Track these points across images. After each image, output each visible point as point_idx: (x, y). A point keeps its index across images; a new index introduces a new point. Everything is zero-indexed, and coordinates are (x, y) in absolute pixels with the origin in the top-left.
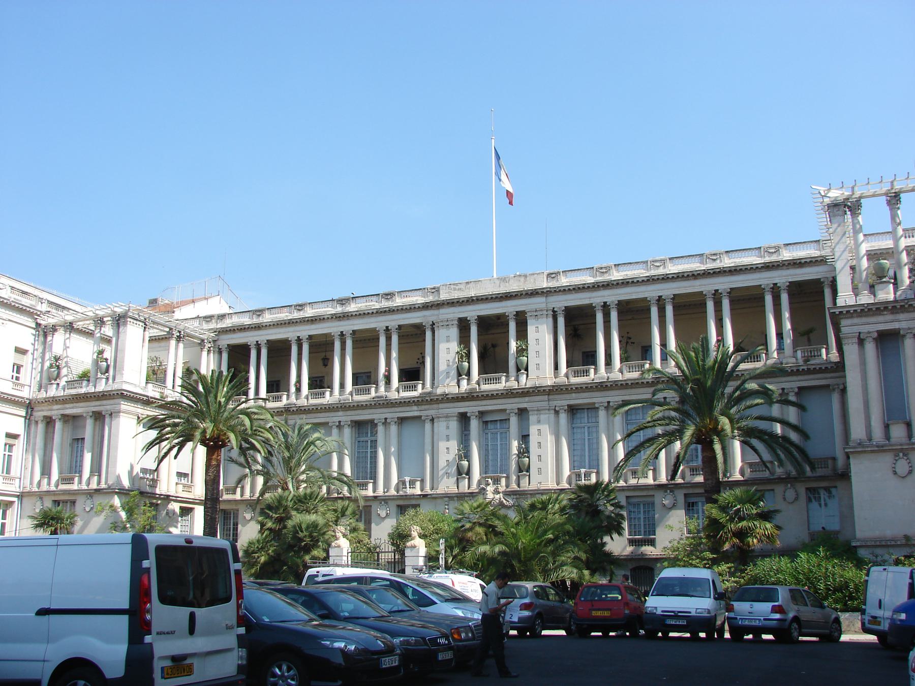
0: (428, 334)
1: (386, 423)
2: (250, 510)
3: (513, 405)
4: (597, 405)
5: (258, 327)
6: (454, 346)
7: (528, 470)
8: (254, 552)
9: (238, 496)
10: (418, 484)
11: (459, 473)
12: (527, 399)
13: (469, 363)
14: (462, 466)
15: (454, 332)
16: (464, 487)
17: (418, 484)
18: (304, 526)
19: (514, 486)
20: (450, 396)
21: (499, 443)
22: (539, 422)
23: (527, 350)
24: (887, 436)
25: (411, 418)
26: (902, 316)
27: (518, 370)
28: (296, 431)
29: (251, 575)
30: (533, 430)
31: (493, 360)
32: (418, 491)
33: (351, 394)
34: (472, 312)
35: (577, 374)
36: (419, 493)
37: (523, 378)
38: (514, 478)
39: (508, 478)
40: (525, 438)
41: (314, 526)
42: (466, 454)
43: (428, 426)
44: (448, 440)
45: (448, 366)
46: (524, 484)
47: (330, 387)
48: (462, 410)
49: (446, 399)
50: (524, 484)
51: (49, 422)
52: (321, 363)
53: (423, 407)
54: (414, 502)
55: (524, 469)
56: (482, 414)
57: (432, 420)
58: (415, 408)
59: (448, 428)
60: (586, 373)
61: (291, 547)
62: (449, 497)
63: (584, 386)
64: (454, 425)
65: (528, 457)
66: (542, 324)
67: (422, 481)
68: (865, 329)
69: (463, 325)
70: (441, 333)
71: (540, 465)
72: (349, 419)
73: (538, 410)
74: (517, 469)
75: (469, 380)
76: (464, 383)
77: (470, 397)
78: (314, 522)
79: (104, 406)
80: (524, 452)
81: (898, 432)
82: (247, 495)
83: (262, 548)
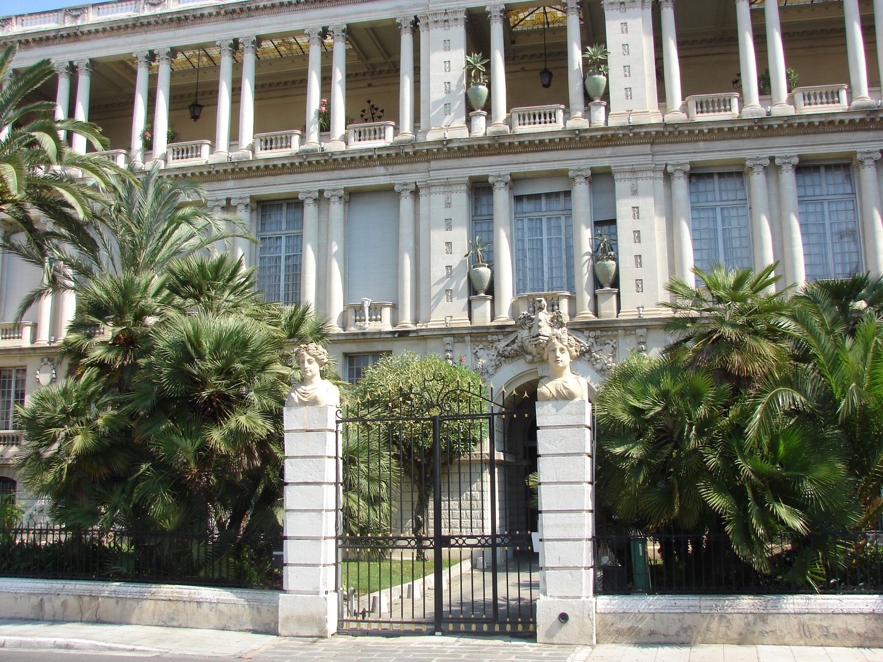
0: (406, 40)
1: (321, 199)
2: (49, 367)
4: (748, 163)
5: (74, 36)
6: (459, 57)
7: (616, 284)
8: (51, 423)
9: (25, 342)
10: (387, 312)
11: (473, 290)
12: (608, 151)
13: (489, 86)
14: (480, 277)
15: (459, 33)
16: (483, 315)
17: (387, 312)
18: (206, 345)
19: (586, 314)
20: (455, 145)
21: (545, 237)
22: (635, 193)
23: (605, 62)
25: (372, 192)
27: (588, 98)
28: (151, 191)
29: (45, 489)
30: (623, 208)
32: (386, 325)
33: (252, 149)
35: (361, 135)
36: (390, 328)
38: (587, 298)
39: (572, 299)
40: (606, 224)
41: (238, 343)
42: (482, 252)
43: (406, 203)
44: (449, 227)
45: (448, 92)
46: (608, 308)
48: (477, 172)
49: (448, 150)
50: (608, 308)
52: (187, 112)
53: (397, 168)
54: (379, 347)
55: (606, 282)
56: (515, 180)
57: (416, 193)
58: (381, 170)
59: (448, 205)
60: (727, 103)
61: (163, 406)
62: (454, 335)
63: (726, 127)
64: (461, 199)
65: (615, 259)
66: (635, 17)
67: (395, 308)
70: (430, 36)
71: (640, 273)
73: (633, 172)
74: (591, 282)
75: (489, 118)
77: (497, 146)
78: (237, 332)
80: (606, 249)
82: (44, 339)
83: (76, 413)
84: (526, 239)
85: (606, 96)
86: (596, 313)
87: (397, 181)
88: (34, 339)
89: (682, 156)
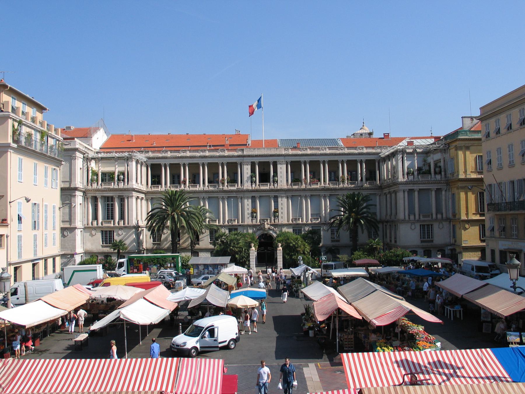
3: (273, 194)
15: (249, 167)
16: (254, 222)
24: (409, 218)
26: (415, 185)
31: (265, 178)
34: (257, 160)
35: (231, 186)
37: (276, 185)
43: (239, 200)
47: (199, 183)
49: (248, 191)
50: (276, 221)
51: (411, 191)
57: (241, 198)
60: (235, 185)
68: (406, 188)
69: (253, 165)
71: (282, 215)
72: (208, 196)
76: (254, 185)
79: (125, 194)
81: (412, 217)
84: (261, 277)
85: (277, 182)
86: (119, 224)
87: (238, 195)
88: (238, 223)
89: (290, 194)
